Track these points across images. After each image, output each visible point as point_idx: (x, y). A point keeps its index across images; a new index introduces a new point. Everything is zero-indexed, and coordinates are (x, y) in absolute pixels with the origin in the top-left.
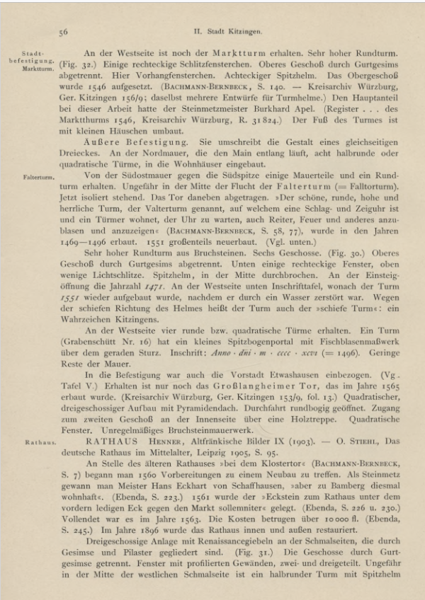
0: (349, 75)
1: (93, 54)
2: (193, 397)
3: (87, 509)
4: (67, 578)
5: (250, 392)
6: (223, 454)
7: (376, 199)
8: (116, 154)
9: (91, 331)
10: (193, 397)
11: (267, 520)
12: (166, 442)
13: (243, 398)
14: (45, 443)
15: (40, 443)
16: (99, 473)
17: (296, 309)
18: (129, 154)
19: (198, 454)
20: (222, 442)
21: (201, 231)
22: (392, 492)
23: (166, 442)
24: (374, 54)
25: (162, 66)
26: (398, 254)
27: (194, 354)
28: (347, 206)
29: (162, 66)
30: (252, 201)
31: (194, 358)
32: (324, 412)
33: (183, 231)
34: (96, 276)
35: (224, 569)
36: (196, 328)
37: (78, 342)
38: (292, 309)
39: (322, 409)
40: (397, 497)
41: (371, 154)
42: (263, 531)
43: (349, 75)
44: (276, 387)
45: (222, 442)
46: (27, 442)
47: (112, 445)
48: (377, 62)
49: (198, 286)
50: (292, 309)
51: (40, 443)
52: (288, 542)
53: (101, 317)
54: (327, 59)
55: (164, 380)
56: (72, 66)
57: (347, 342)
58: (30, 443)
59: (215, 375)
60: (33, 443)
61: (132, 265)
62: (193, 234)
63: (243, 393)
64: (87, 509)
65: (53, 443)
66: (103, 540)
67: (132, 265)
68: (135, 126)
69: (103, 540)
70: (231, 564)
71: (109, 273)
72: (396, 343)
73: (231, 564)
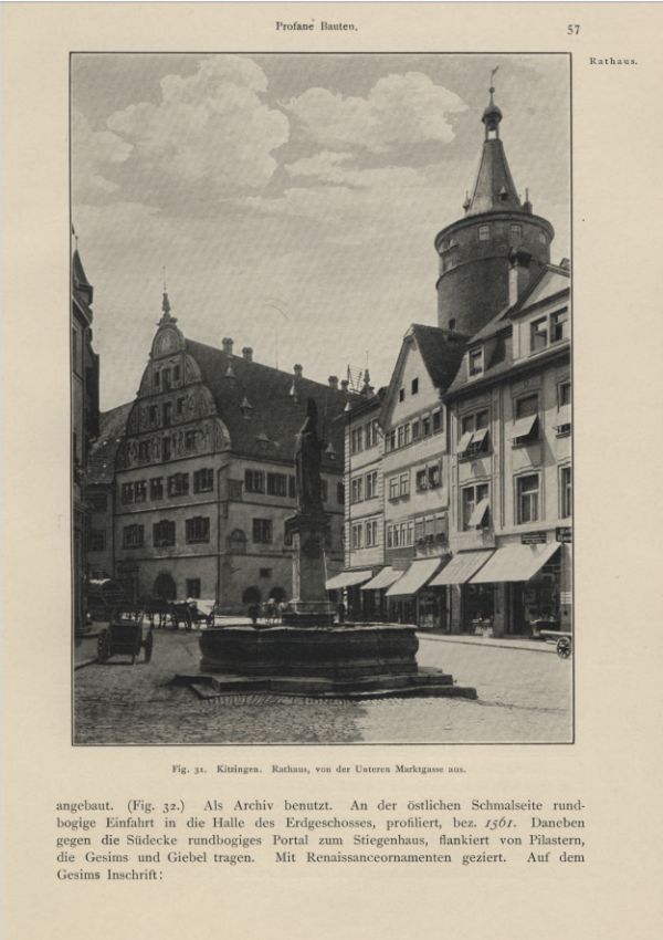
1: (365, 806)
7: (240, 824)
8: (360, 807)
9: (360, 807)
11: (64, 824)
14: (620, 63)
15: (613, 62)
20: (468, 841)
22: (573, 850)
32: (240, 847)
39: (238, 842)
41: (412, 806)
45: (468, 841)
48: (315, 819)
51: (613, 62)
55: (466, 813)
56: (148, 808)
57: (149, 841)
59: (383, 806)
60: (601, 63)
65: (633, 62)
66: (242, 838)
69: (242, 838)
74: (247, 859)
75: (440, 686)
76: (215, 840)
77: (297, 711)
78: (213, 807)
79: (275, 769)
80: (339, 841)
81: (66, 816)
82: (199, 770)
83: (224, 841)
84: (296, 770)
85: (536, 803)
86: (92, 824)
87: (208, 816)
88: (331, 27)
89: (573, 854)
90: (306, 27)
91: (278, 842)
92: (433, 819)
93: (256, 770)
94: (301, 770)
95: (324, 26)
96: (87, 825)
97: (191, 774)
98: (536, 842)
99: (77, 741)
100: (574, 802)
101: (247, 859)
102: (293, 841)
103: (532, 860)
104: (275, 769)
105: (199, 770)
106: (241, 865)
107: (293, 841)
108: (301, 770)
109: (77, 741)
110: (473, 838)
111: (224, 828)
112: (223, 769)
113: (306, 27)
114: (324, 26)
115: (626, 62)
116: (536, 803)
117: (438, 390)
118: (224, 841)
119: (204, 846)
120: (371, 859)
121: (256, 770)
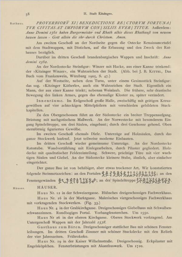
0: (128, 43)
2: (57, 148)
6: (44, 130)
10: (57, 148)
14: (18, 24)
16: (47, 167)
17: (120, 125)
18: (77, 222)
24: (51, 181)
25: (73, 106)
27: (154, 57)
28: (54, 157)
29: (73, 106)
30: (44, 205)
31: (154, 59)
32: (72, 215)
35: (115, 196)
36: (50, 179)
37: (58, 48)
38: (118, 125)
43: (128, 43)
46: (11, 23)
47: (39, 200)
49: (32, 236)
50: (118, 125)
53: (70, 119)
58: (12, 23)
60: (13, 24)
61: (72, 208)
67: (72, 208)
68: (70, 83)
69: (91, 226)
70: (127, 208)
72: (54, 139)
73: (127, 208)
76: (86, 153)
78: (125, 72)
80: (107, 144)
81: (168, 156)
83: (68, 213)
85: (103, 42)
86: (132, 153)
87: (107, 69)
89: (53, 180)
91: (81, 213)
92: (162, 94)
96: (131, 154)
98: (130, 149)
100: (168, 66)
102: (93, 174)
107: (93, 174)
110: (156, 152)
111: (108, 102)
115: (20, 24)
116: (103, 42)
118: (68, 213)
119: (57, 92)
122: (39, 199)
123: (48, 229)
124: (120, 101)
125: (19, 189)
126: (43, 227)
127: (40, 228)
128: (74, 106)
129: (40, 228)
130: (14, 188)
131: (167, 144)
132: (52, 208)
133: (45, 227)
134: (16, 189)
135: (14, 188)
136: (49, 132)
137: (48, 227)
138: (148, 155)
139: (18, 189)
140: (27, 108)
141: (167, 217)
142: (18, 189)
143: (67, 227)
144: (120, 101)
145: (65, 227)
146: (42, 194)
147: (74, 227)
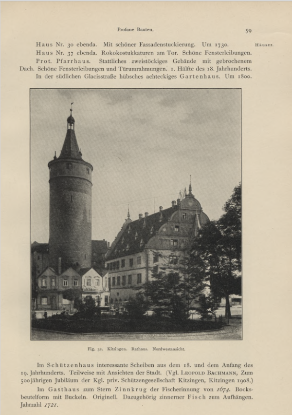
3: (176, 398)
4: (233, 79)
5: (218, 377)
9: (226, 366)
12: (232, 373)
13: (183, 381)
19: (182, 374)
21: (229, 373)
23: (232, 373)
26: (252, 366)
29: (155, 62)
33: (216, 373)
34: (183, 373)
40: (251, 373)
42: (132, 373)
44: (122, 390)
52: (135, 373)
54: (205, 369)
62: (223, 375)
63: (213, 378)
64: (176, 398)
71: (125, 371)
74: (250, 397)
75: (229, 325)
77: (134, 335)
79: (133, 349)
82: (100, 350)
84: (142, 349)
88: (142, 30)
90: (130, 30)
93: (125, 349)
94: (144, 349)
95: (138, 29)
97: (96, 351)
99: (32, 339)
101: (250, 397)
103: (224, 366)
104: (133, 349)
105: (100, 350)
106: (247, 401)
108: (144, 349)
109: (32, 339)
112: (110, 349)
113: (130, 30)
114: (138, 29)
117: (225, 213)
120: (190, 373)
121: (125, 349)
122: (38, 45)
123: (66, 392)
124: (136, 62)
125: (265, 47)
126: (57, 390)
127: (52, 390)
128: (157, 62)
129: (52, 390)
130: (257, 45)
131: (162, 77)
132: (60, 45)
133: (61, 390)
134: (261, 46)
135: (257, 45)
136: (191, 65)
137: (66, 390)
138: (148, 71)
139: (264, 45)
140: (218, 65)
141: (223, 364)
142: (264, 45)
143: (206, 373)
144: (136, 62)
145: (203, 373)
146: (44, 45)
147: (68, 61)
